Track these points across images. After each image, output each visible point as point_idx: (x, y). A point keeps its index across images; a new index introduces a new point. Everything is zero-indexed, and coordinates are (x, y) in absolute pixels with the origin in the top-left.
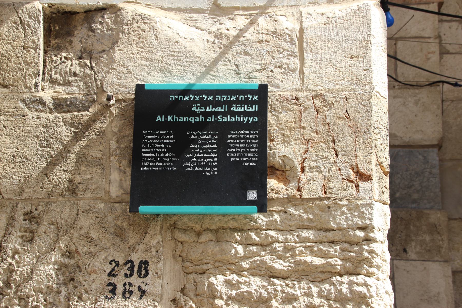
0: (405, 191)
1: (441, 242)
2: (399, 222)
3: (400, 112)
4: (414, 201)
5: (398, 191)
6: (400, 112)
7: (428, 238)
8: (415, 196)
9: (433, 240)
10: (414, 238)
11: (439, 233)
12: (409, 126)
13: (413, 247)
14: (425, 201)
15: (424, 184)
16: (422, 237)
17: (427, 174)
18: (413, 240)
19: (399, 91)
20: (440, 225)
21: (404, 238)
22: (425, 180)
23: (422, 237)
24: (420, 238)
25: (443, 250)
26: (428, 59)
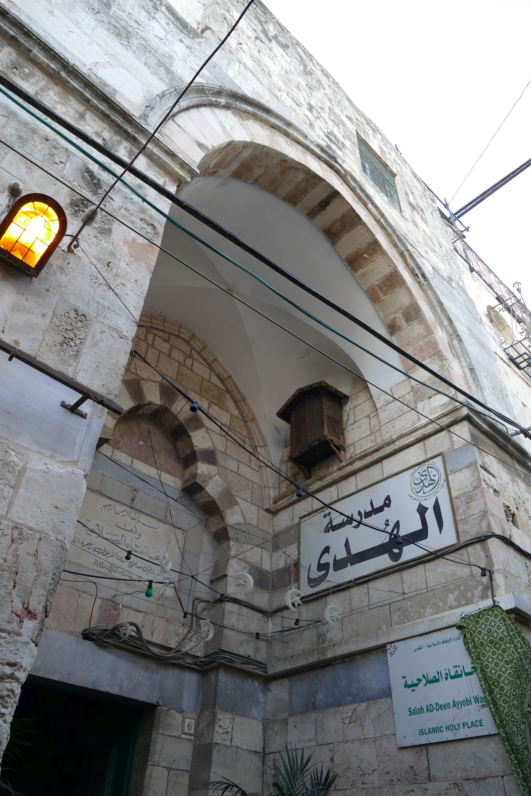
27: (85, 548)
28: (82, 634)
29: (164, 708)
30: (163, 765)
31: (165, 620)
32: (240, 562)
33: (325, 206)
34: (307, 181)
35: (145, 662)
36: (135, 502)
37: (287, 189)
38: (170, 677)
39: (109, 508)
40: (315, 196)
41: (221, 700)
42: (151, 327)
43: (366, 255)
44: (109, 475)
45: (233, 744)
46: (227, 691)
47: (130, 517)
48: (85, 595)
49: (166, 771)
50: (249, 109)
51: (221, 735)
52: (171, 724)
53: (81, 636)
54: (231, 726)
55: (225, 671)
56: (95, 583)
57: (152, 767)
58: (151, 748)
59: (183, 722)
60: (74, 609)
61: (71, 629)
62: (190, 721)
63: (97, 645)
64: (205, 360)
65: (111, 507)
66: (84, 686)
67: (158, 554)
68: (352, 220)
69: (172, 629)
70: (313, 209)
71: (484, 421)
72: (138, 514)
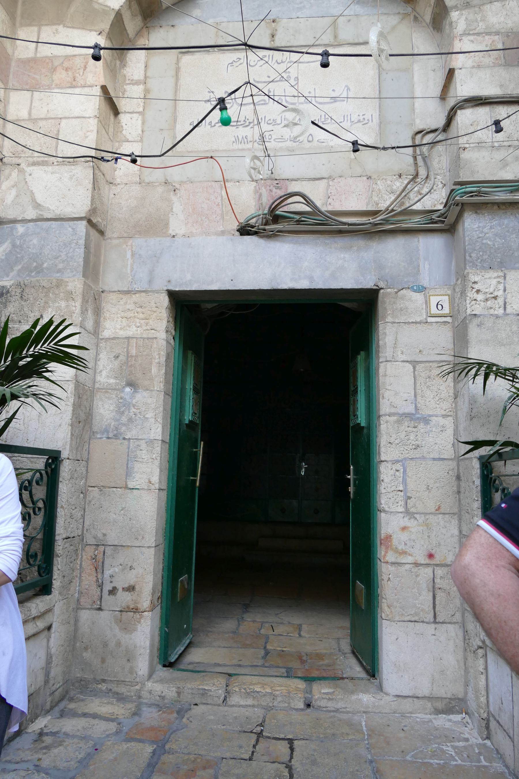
0: (52, 262)
1: (74, 308)
2: (41, 290)
3: (56, 187)
4: (59, 271)
5: (46, 261)
6: (56, 187)
7: (63, 304)
8: (61, 266)
9: (67, 306)
10: (51, 305)
11: (73, 300)
12: (62, 200)
13: (49, 313)
14: (69, 271)
15: (70, 255)
16: (59, 303)
17: (73, 245)
18: (49, 307)
19: (57, 167)
20: (75, 292)
21: (42, 305)
22: (71, 250)
23: (59, 303)
24: (57, 305)
25: (75, 315)
26: (87, 137)
28: (237, 231)
29: (389, 290)
30: (402, 359)
31: (365, 178)
32: (479, 38)
35: (341, 241)
36: (276, 38)
38: (392, 251)
39: (239, 63)
41: (473, 255)
44: (225, 20)
45: (508, 311)
46: (484, 241)
47: (274, 61)
49: (410, 367)
51: (482, 303)
52: (407, 308)
53: (238, 233)
54: (501, 287)
55: (476, 213)
56: (212, 157)
57: (385, 363)
58: (381, 342)
59: (427, 303)
60: (218, 205)
61: (221, 228)
62: (439, 298)
63: (262, 237)
65: (242, 61)
69: (381, 188)
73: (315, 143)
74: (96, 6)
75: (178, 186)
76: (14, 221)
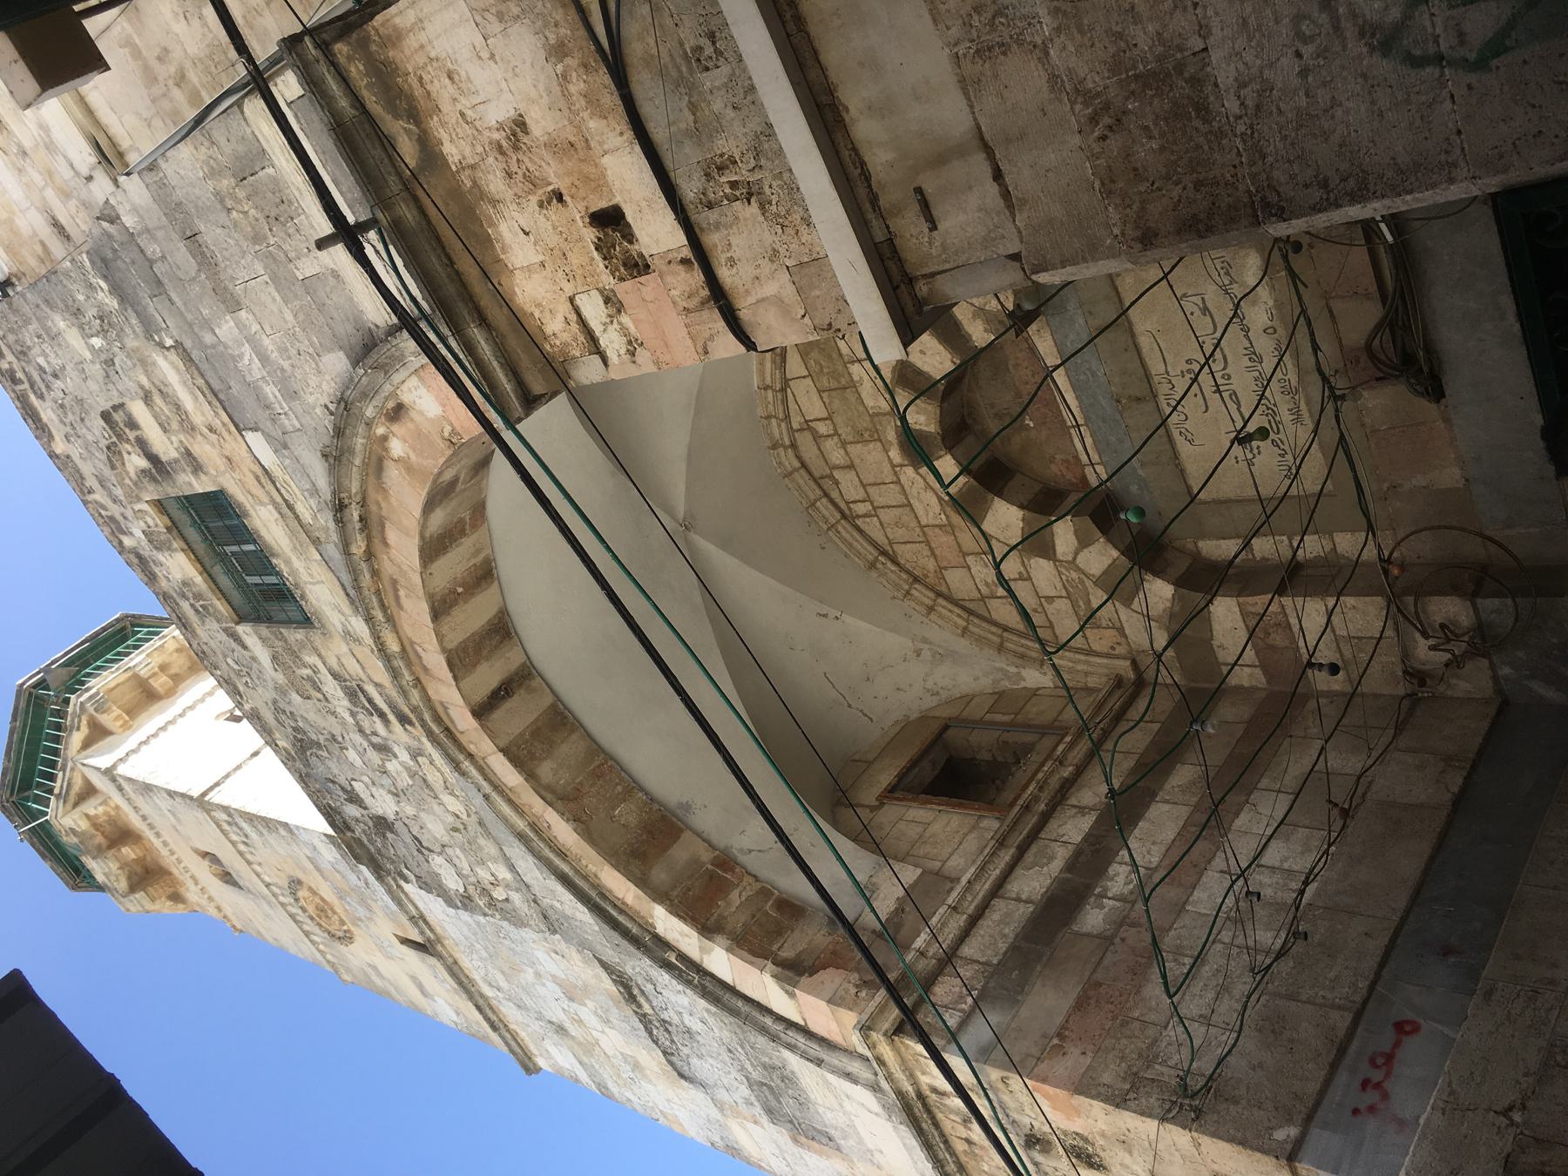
27: (1287, 447)
33: (500, 689)
34: (532, 756)
37: (570, 748)
40: (519, 714)
42: (844, 516)
43: (460, 590)
48: (1367, 420)
50: (621, 918)
61: (1440, 424)
64: (785, 401)
66: (1529, 371)
67: (1197, 313)
68: (566, 800)
70: (520, 685)
71: (469, 348)
72: (1156, 379)
73: (1276, 323)
74: (1177, 609)
75: (1386, 485)
76: (1495, 678)
